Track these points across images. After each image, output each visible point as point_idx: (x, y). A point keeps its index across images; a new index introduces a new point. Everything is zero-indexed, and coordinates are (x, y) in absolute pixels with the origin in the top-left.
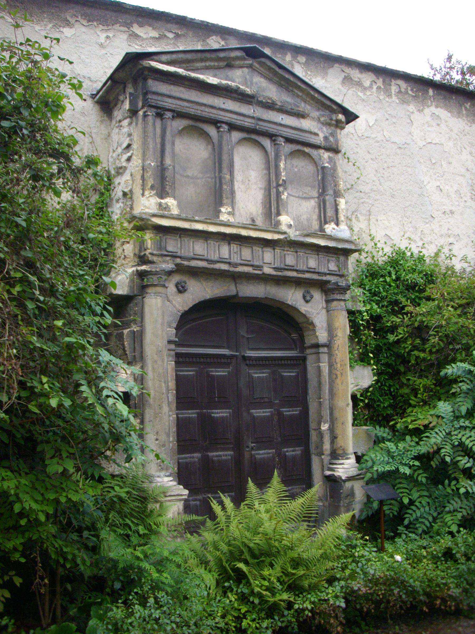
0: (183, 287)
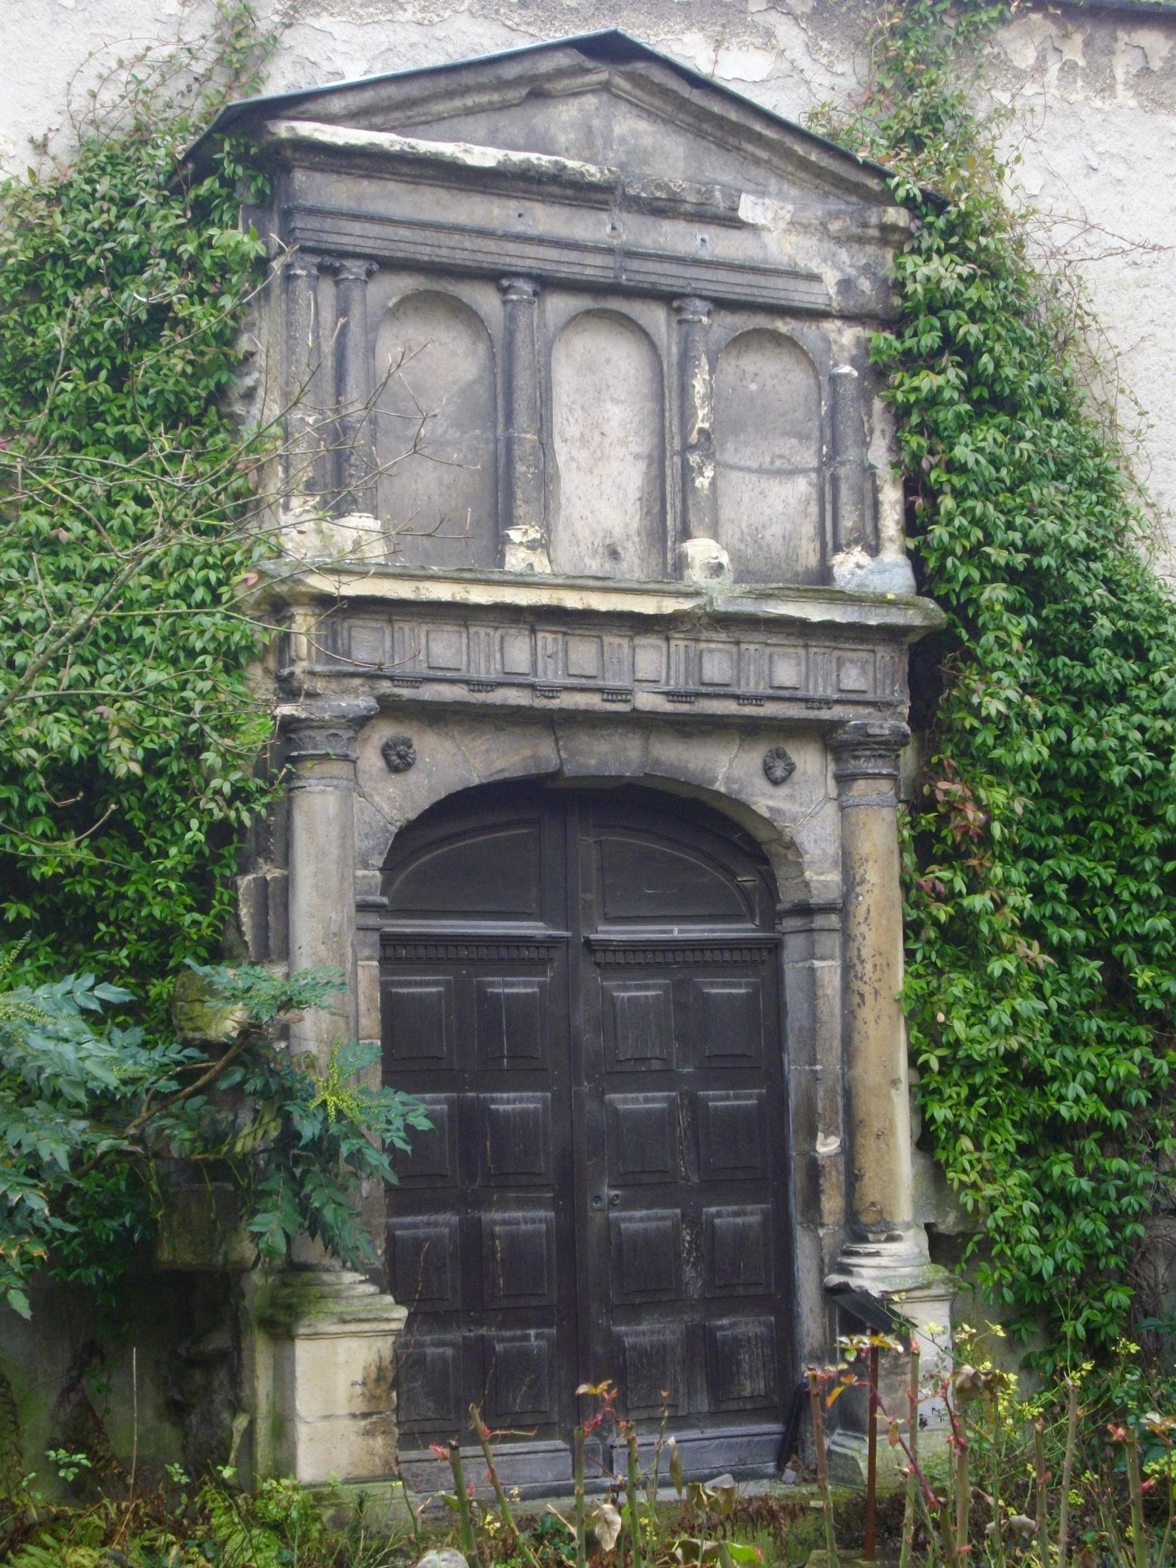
0: (401, 757)
